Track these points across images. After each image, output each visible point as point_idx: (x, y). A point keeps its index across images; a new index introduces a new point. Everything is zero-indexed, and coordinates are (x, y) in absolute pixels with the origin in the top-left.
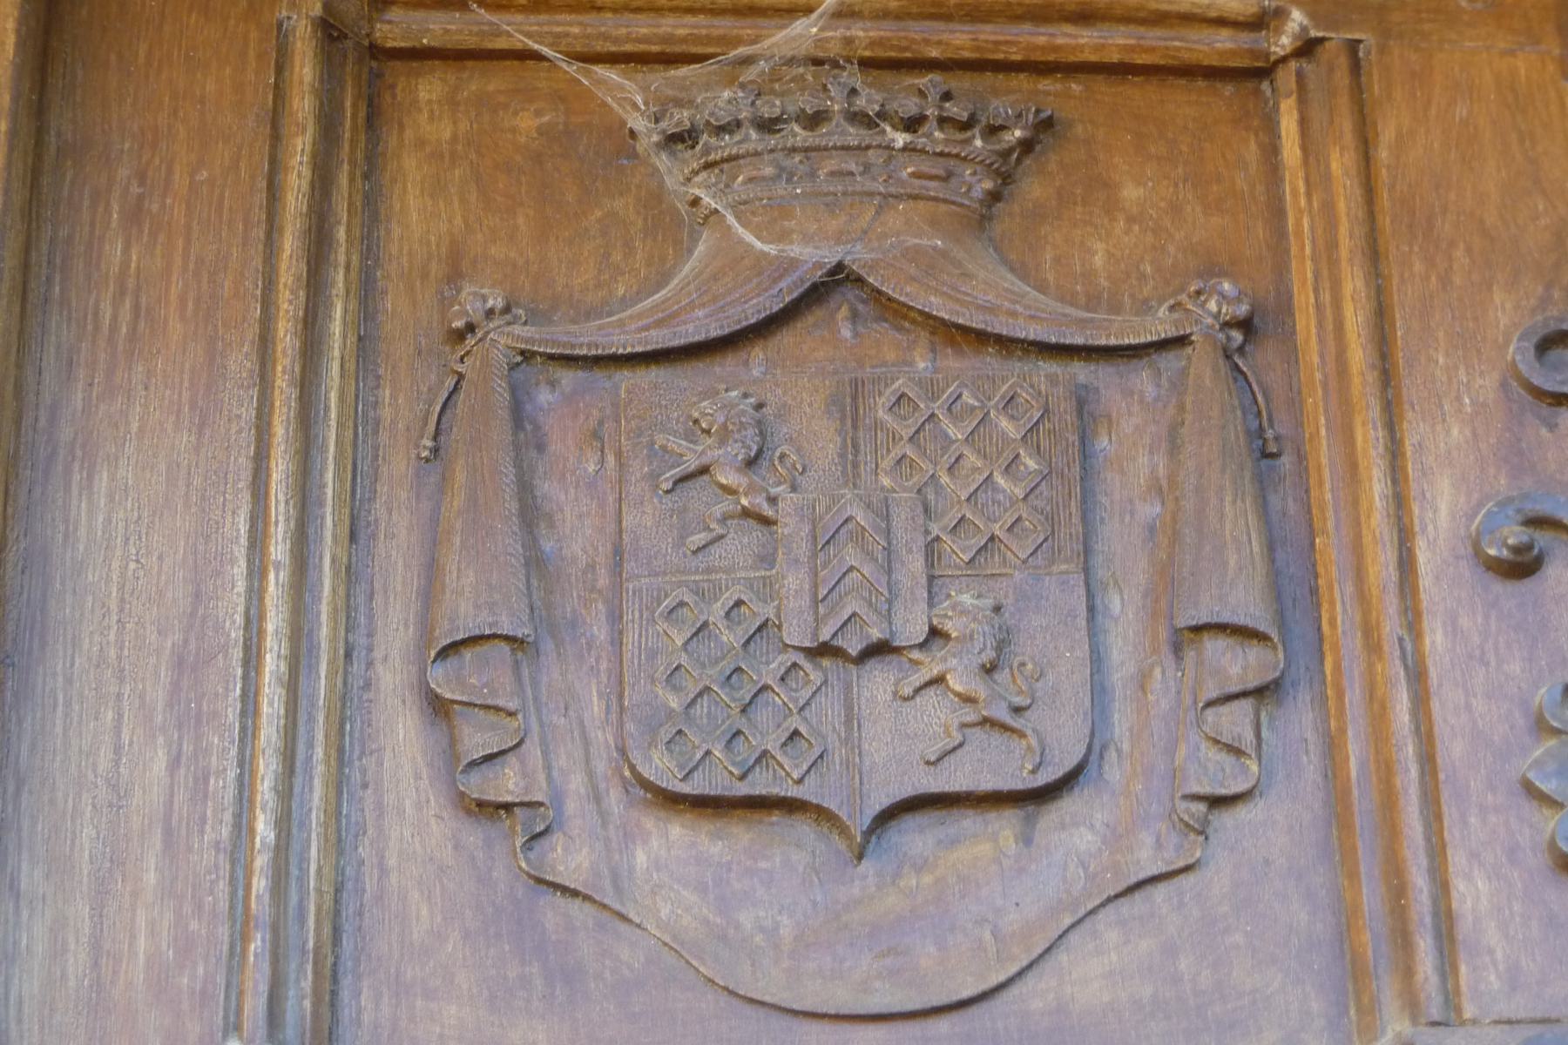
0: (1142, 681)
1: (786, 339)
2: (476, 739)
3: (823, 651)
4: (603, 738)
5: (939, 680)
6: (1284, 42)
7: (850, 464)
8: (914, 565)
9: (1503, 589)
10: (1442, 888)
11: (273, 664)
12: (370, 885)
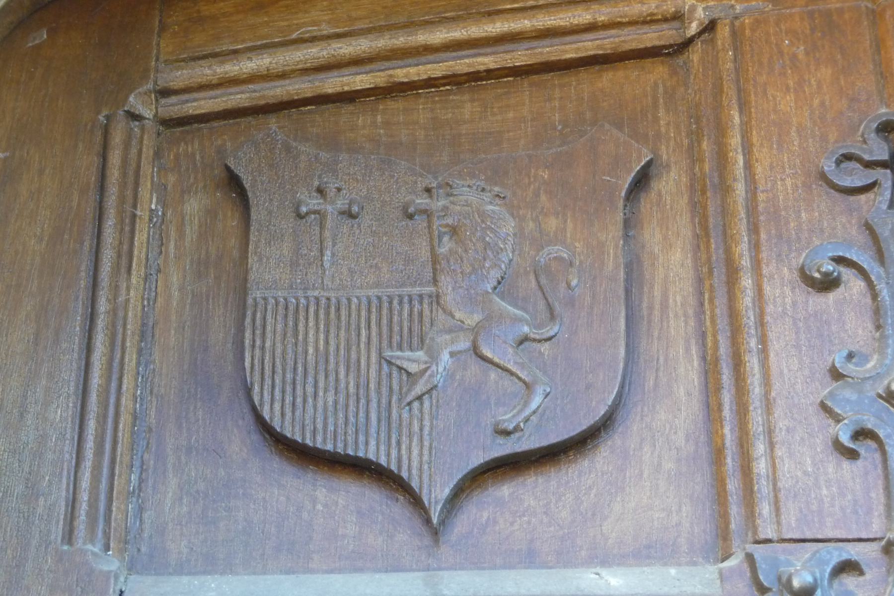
7: (463, 280)
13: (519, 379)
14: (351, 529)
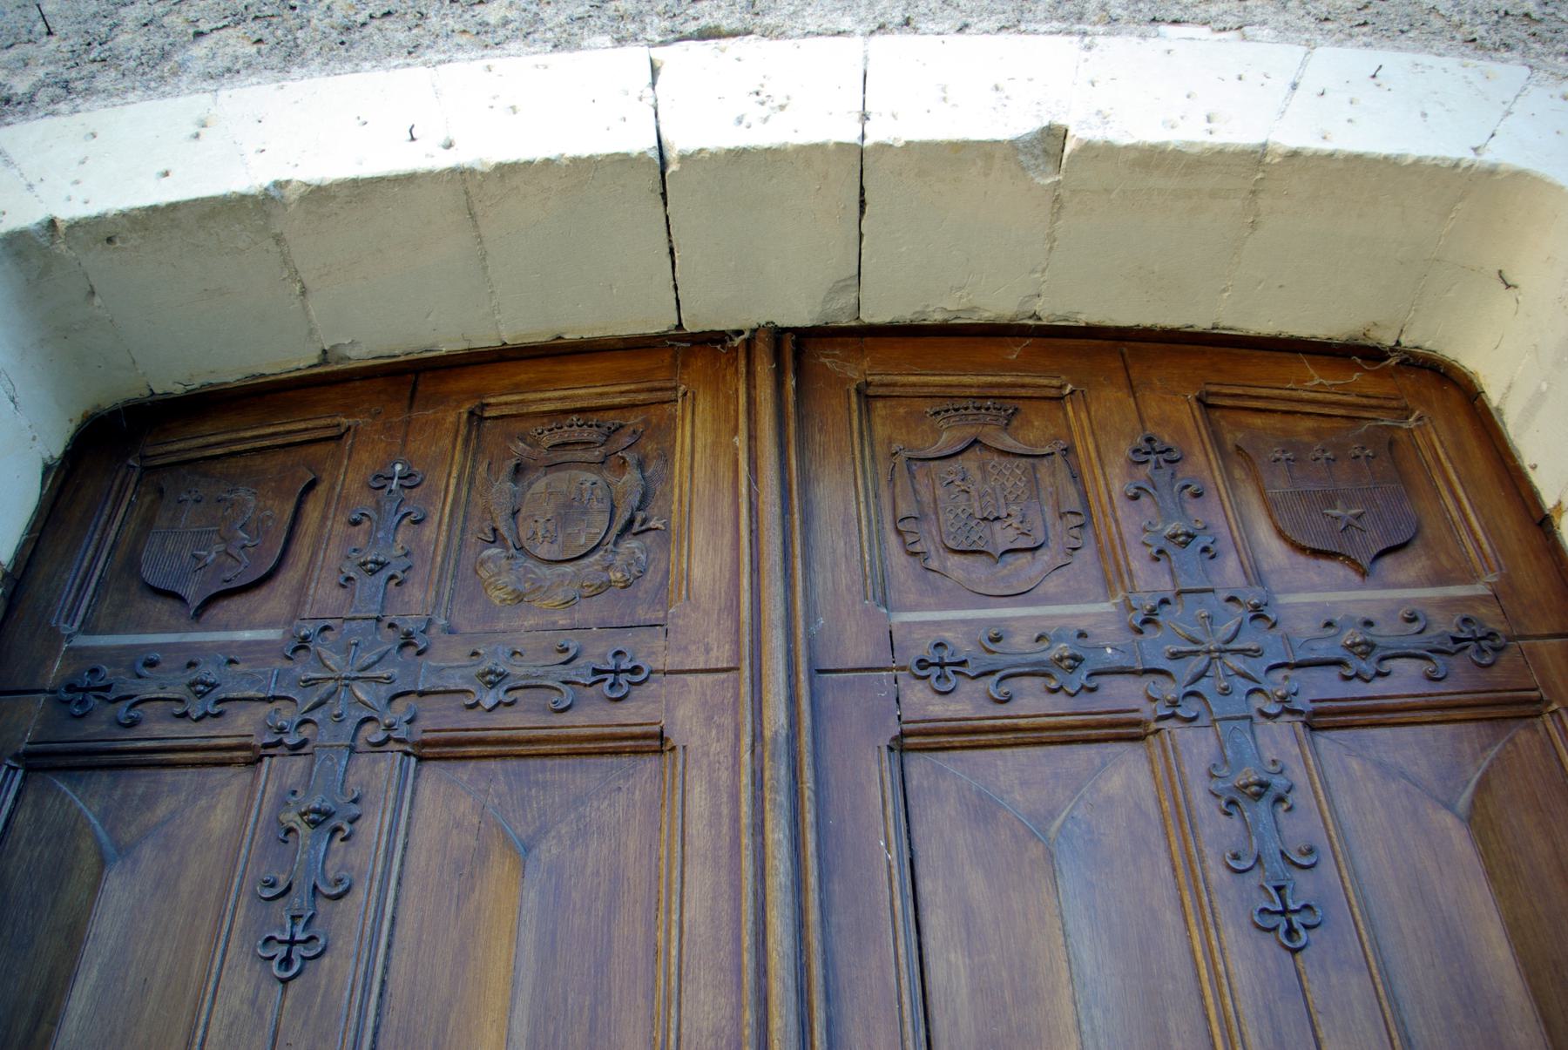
0: (1054, 525)
1: (966, 455)
2: (910, 539)
3: (985, 519)
4: (937, 539)
5: (1010, 525)
6: (1067, 391)
7: (984, 479)
8: (1002, 501)
9: (1134, 503)
10: (1128, 565)
11: (864, 523)
12: (890, 570)
13: (833, 576)
14: (166, 618)
